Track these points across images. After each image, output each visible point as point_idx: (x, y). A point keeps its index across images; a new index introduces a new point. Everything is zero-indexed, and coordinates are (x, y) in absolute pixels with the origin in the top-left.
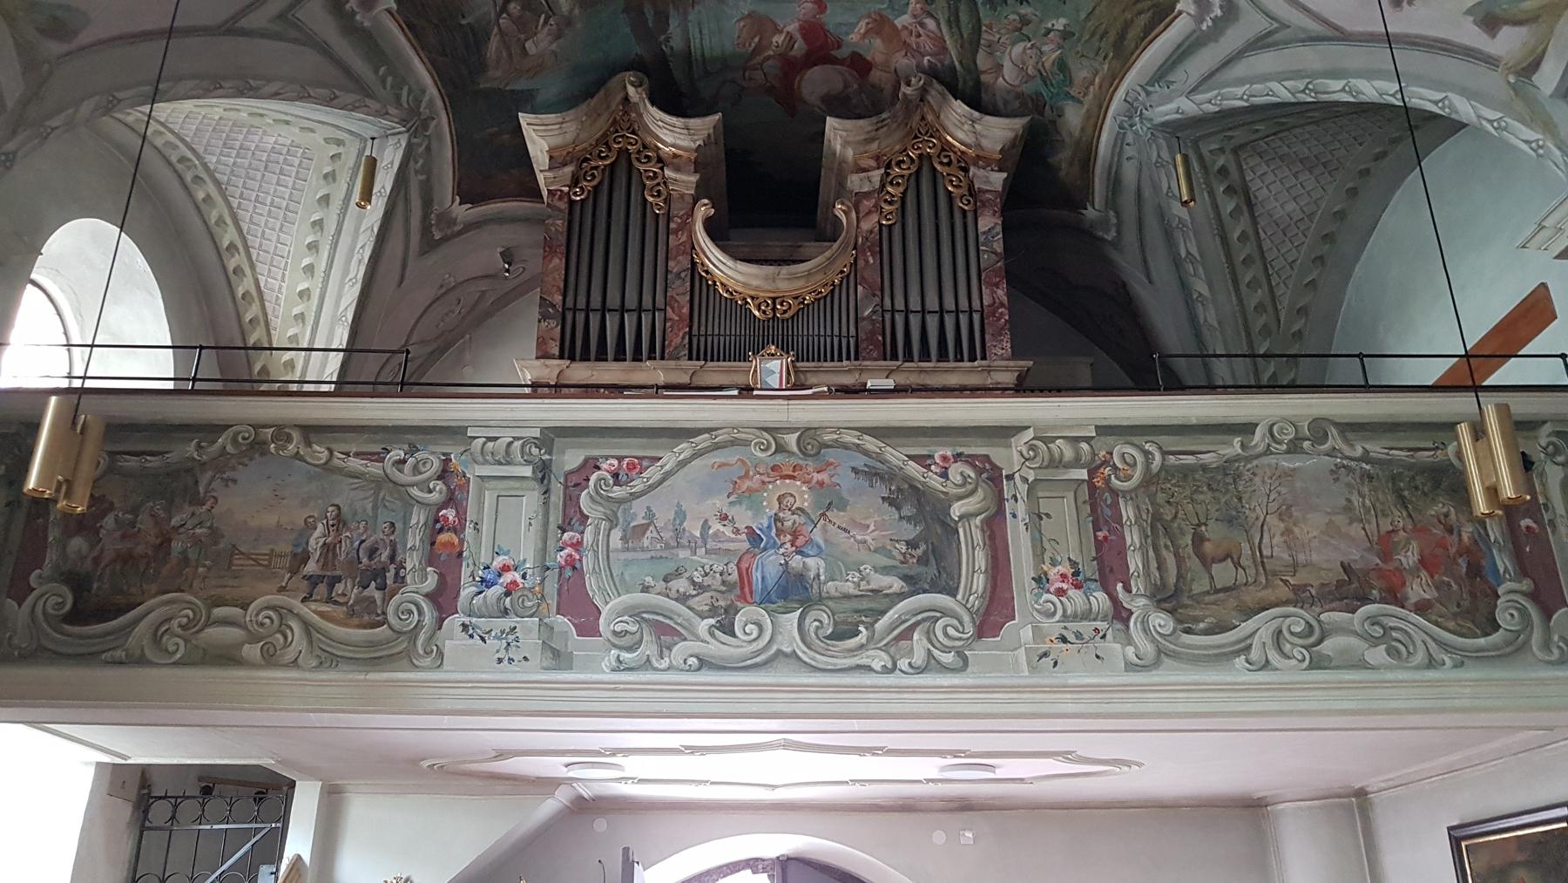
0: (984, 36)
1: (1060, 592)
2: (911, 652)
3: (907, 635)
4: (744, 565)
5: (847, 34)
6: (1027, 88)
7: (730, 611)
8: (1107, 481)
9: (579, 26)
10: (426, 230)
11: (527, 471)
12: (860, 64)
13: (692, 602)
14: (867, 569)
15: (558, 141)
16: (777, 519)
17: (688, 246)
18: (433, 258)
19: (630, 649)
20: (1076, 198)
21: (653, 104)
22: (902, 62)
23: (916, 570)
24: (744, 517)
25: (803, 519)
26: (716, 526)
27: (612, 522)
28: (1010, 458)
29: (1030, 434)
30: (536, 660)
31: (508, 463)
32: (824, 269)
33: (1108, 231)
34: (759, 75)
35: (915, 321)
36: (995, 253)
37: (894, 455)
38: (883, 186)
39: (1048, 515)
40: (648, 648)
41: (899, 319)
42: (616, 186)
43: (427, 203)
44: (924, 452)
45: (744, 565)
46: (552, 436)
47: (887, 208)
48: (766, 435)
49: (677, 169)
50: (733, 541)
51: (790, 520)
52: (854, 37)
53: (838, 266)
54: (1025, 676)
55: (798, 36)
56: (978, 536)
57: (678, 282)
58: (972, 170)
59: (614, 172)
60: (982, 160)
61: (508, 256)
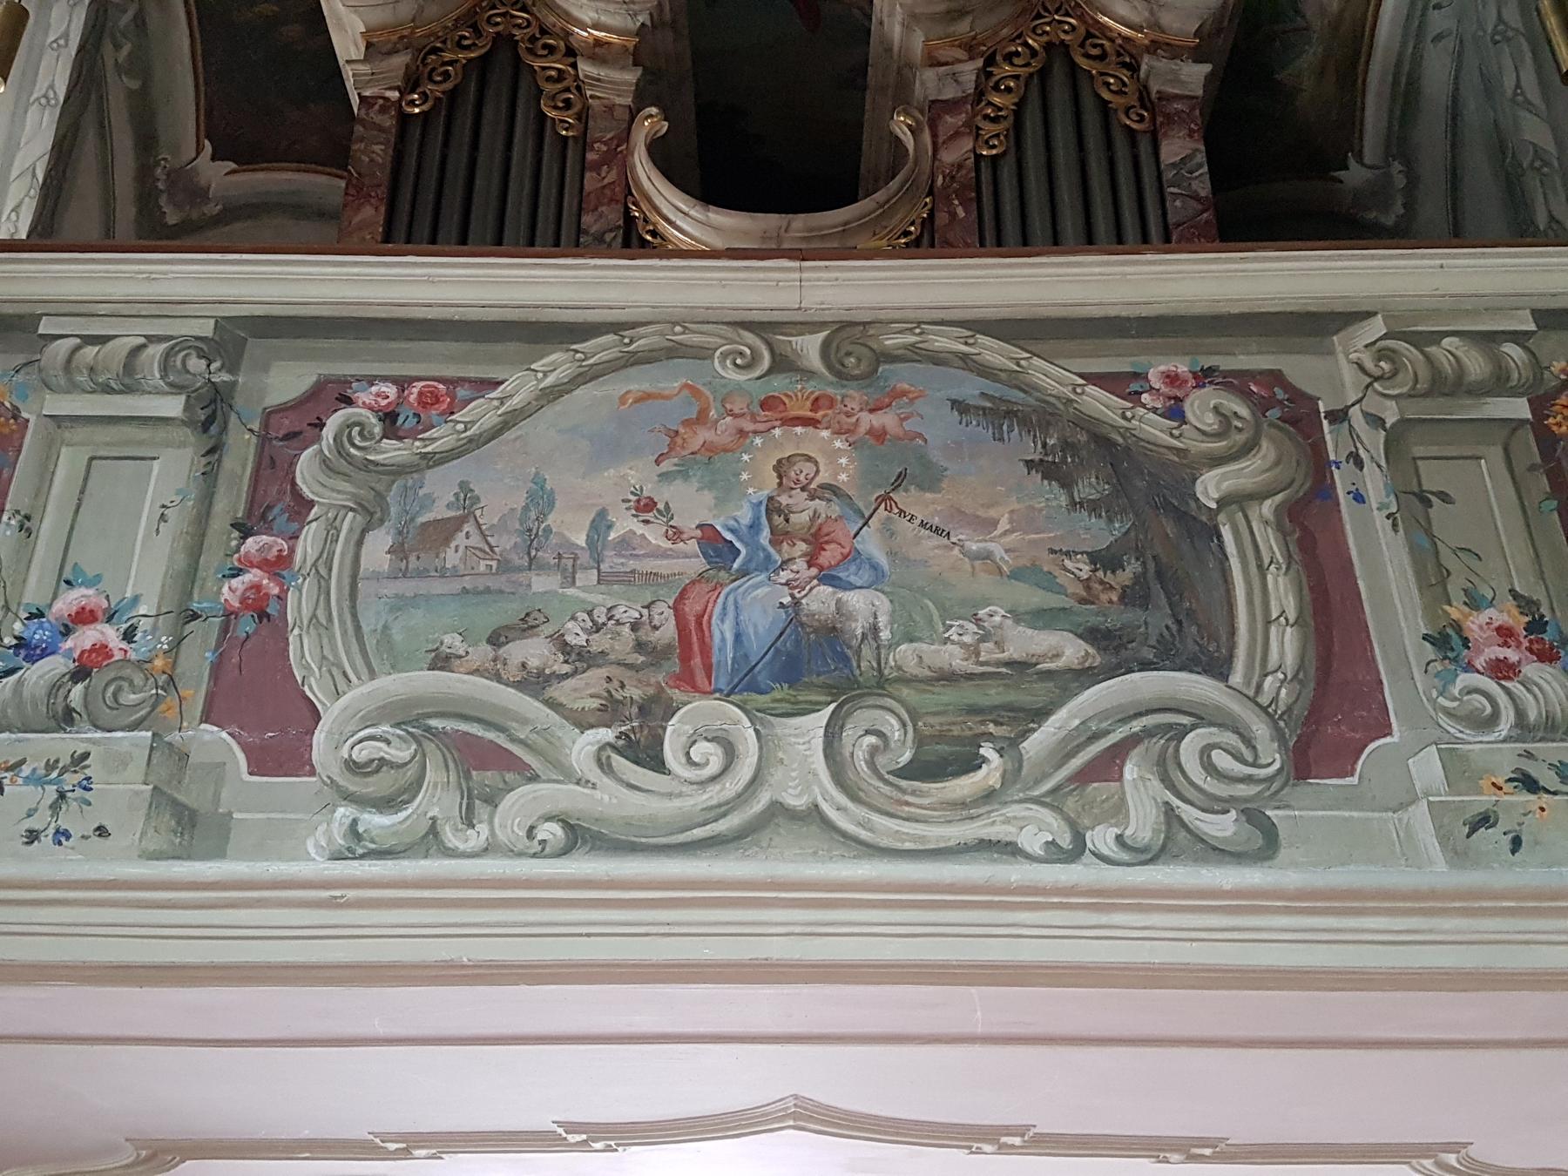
1: (1502, 670)
2: (1118, 811)
3: (1108, 766)
4: (692, 608)
7: (656, 710)
11: (173, 407)
13: (558, 691)
14: (996, 615)
15: (381, 16)
19: (387, 804)
23: (1117, 618)
24: (693, 505)
25: (835, 509)
26: (625, 524)
27: (371, 514)
28: (1338, 386)
30: (128, 834)
31: (128, 390)
37: (1052, 376)
38: (980, 94)
39: (1444, 497)
40: (437, 799)
43: (147, 142)
45: (692, 608)
46: (239, 336)
47: (988, 128)
48: (749, 337)
51: (803, 511)
54: (1439, 873)
56: (1270, 542)
58: (1146, 62)
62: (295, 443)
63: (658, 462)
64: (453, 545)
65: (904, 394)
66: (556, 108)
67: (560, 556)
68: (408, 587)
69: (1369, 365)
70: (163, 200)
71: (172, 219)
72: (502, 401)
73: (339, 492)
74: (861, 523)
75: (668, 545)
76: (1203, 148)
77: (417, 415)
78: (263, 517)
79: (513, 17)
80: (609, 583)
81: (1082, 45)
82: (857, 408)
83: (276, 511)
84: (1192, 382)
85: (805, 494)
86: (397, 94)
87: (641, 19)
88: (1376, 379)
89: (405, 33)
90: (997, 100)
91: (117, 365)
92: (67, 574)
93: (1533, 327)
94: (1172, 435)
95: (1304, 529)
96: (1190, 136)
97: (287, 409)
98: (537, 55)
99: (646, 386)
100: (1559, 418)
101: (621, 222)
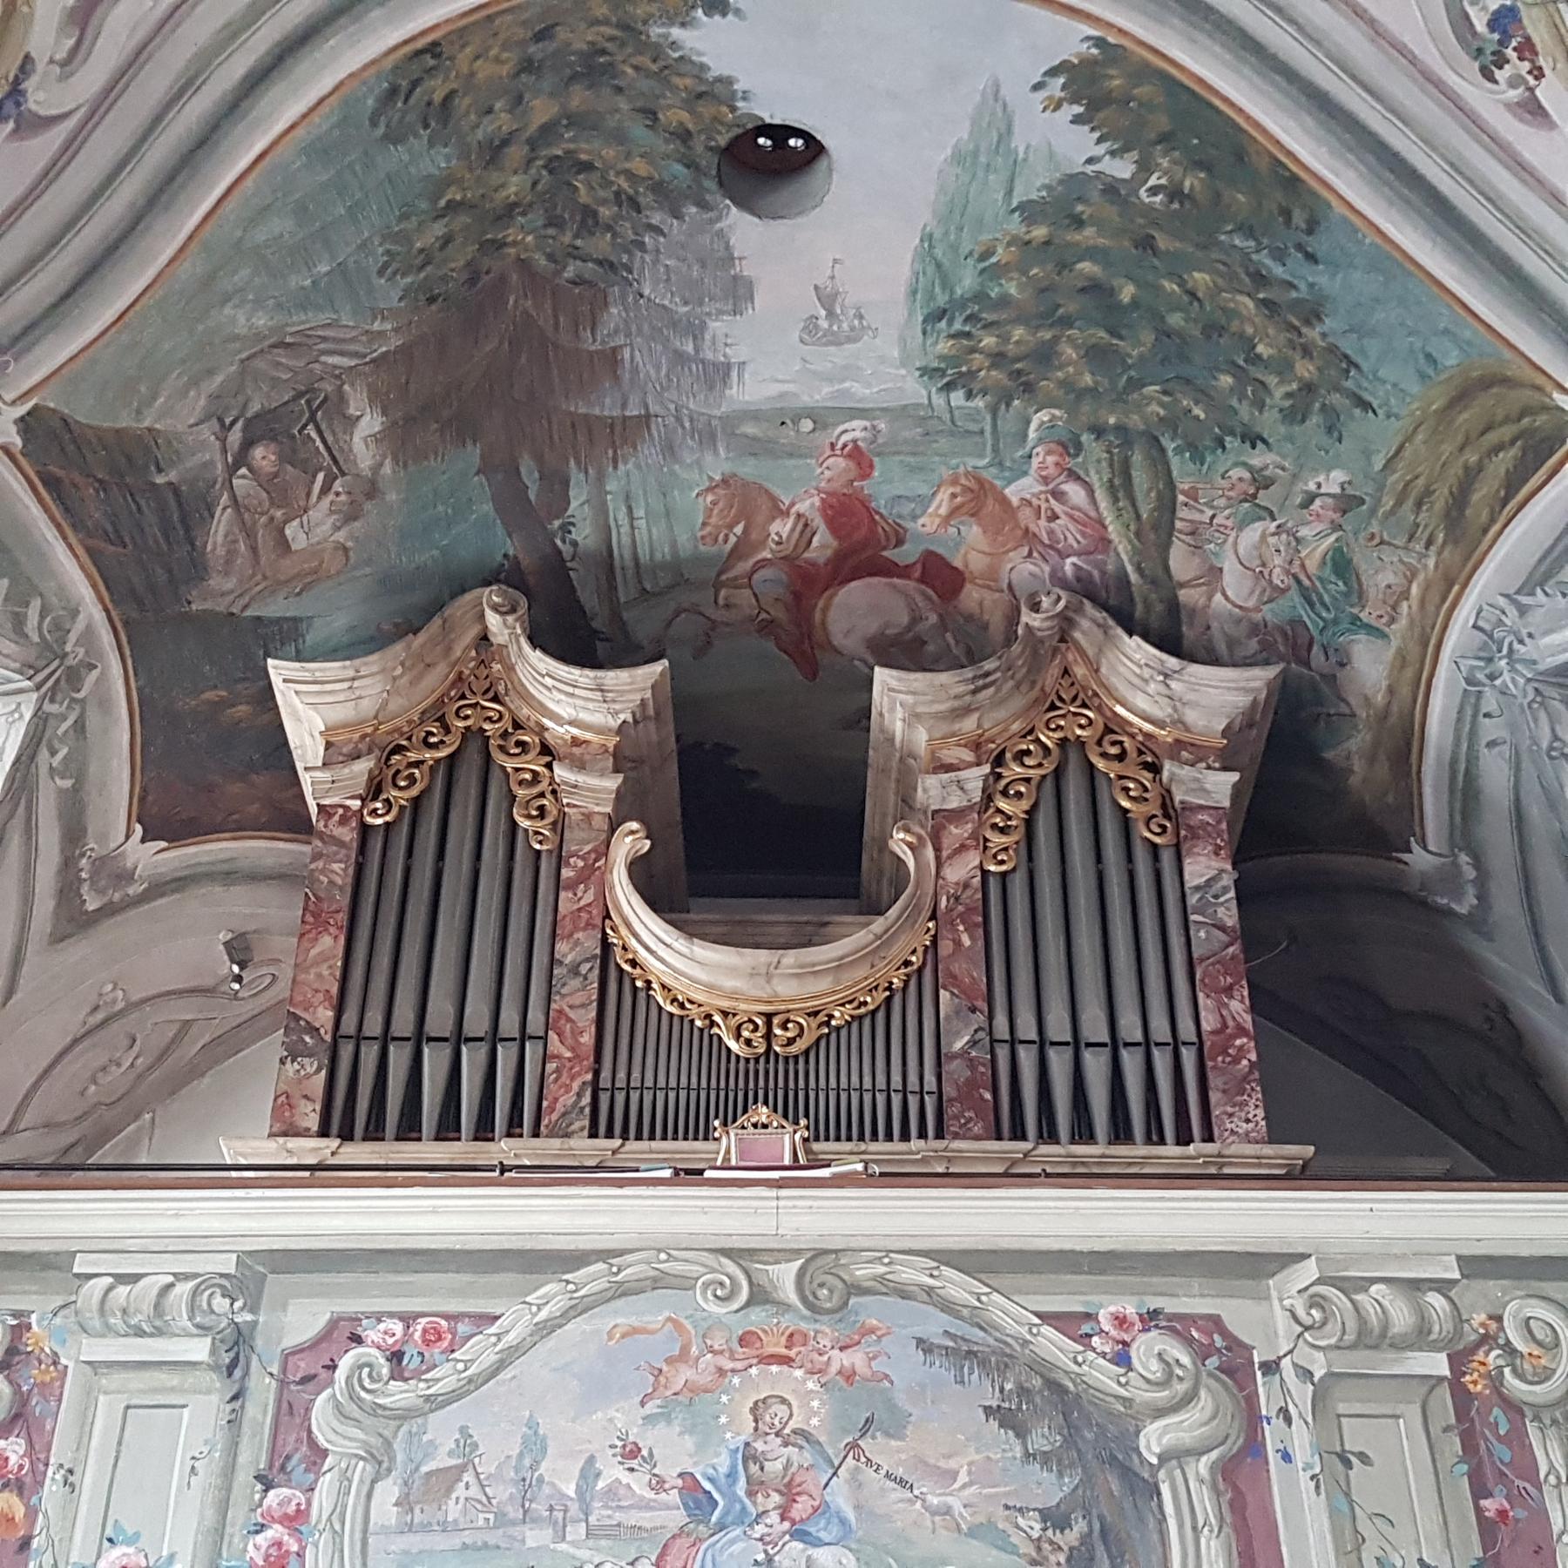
0: (1182, 513)
5: (915, 518)
6: (1268, 613)
8: (1496, 1381)
9: (392, 497)
10: (68, 891)
11: (199, 1349)
12: (940, 576)
16: (750, 1456)
17: (596, 912)
18: (79, 950)
20: (1385, 832)
21: (535, 646)
22: (1023, 569)
24: (675, 1451)
25: (807, 1457)
26: (612, 1472)
27: (380, 1461)
29: (1308, 1272)
31: (159, 1332)
32: (871, 955)
33: (1458, 895)
34: (744, 597)
35: (1059, 1063)
36: (1222, 928)
37: (1012, 1313)
38: (988, 798)
39: (1364, 1458)
41: (1027, 1058)
42: (457, 797)
43: (74, 835)
44: (1074, 1305)
47: (997, 840)
49: (580, 765)
50: (647, 1506)
51: (778, 1458)
52: (927, 523)
53: (898, 951)
55: (818, 522)
56: (1205, 1502)
57: (575, 983)
58: (1168, 768)
59: (455, 773)
60: (1188, 749)
61: (240, 950)
62: (310, 1386)
63: (643, 1404)
64: (454, 1496)
65: (872, 1331)
66: (529, 817)
67: (551, 1509)
68: (414, 1542)
69: (1301, 1313)
70: (85, 888)
71: (91, 906)
72: (499, 1336)
73: (350, 1439)
74: (831, 1471)
75: (652, 1495)
76: (1229, 867)
77: (421, 1354)
78: (283, 1468)
79: (484, 708)
80: (597, 1537)
81: (1099, 743)
82: (829, 1345)
83: (294, 1461)
84: (1138, 1326)
85: (779, 1440)
86: (358, 803)
87: (622, 717)
88: (1307, 1328)
89: (369, 730)
90: (1002, 804)
91: (147, 1307)
92: (109, 1532)
93: (1457, 1275)
94: (1119, 1383)
95: (1236, 1489)
96: (1217, 854)
97: (302, 1350)
98: (509, 754)
99: (634, 1321)
100: (1476, 1375)
101: (598, 951)
